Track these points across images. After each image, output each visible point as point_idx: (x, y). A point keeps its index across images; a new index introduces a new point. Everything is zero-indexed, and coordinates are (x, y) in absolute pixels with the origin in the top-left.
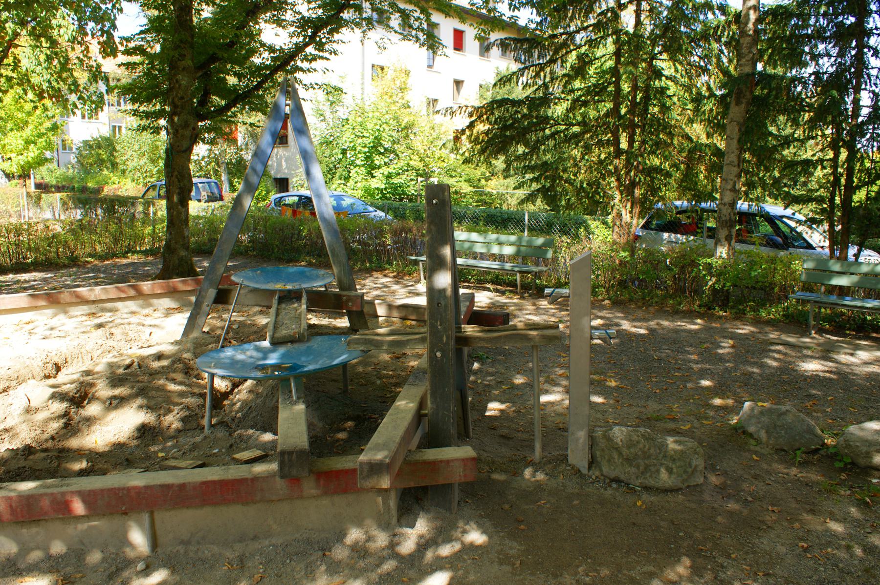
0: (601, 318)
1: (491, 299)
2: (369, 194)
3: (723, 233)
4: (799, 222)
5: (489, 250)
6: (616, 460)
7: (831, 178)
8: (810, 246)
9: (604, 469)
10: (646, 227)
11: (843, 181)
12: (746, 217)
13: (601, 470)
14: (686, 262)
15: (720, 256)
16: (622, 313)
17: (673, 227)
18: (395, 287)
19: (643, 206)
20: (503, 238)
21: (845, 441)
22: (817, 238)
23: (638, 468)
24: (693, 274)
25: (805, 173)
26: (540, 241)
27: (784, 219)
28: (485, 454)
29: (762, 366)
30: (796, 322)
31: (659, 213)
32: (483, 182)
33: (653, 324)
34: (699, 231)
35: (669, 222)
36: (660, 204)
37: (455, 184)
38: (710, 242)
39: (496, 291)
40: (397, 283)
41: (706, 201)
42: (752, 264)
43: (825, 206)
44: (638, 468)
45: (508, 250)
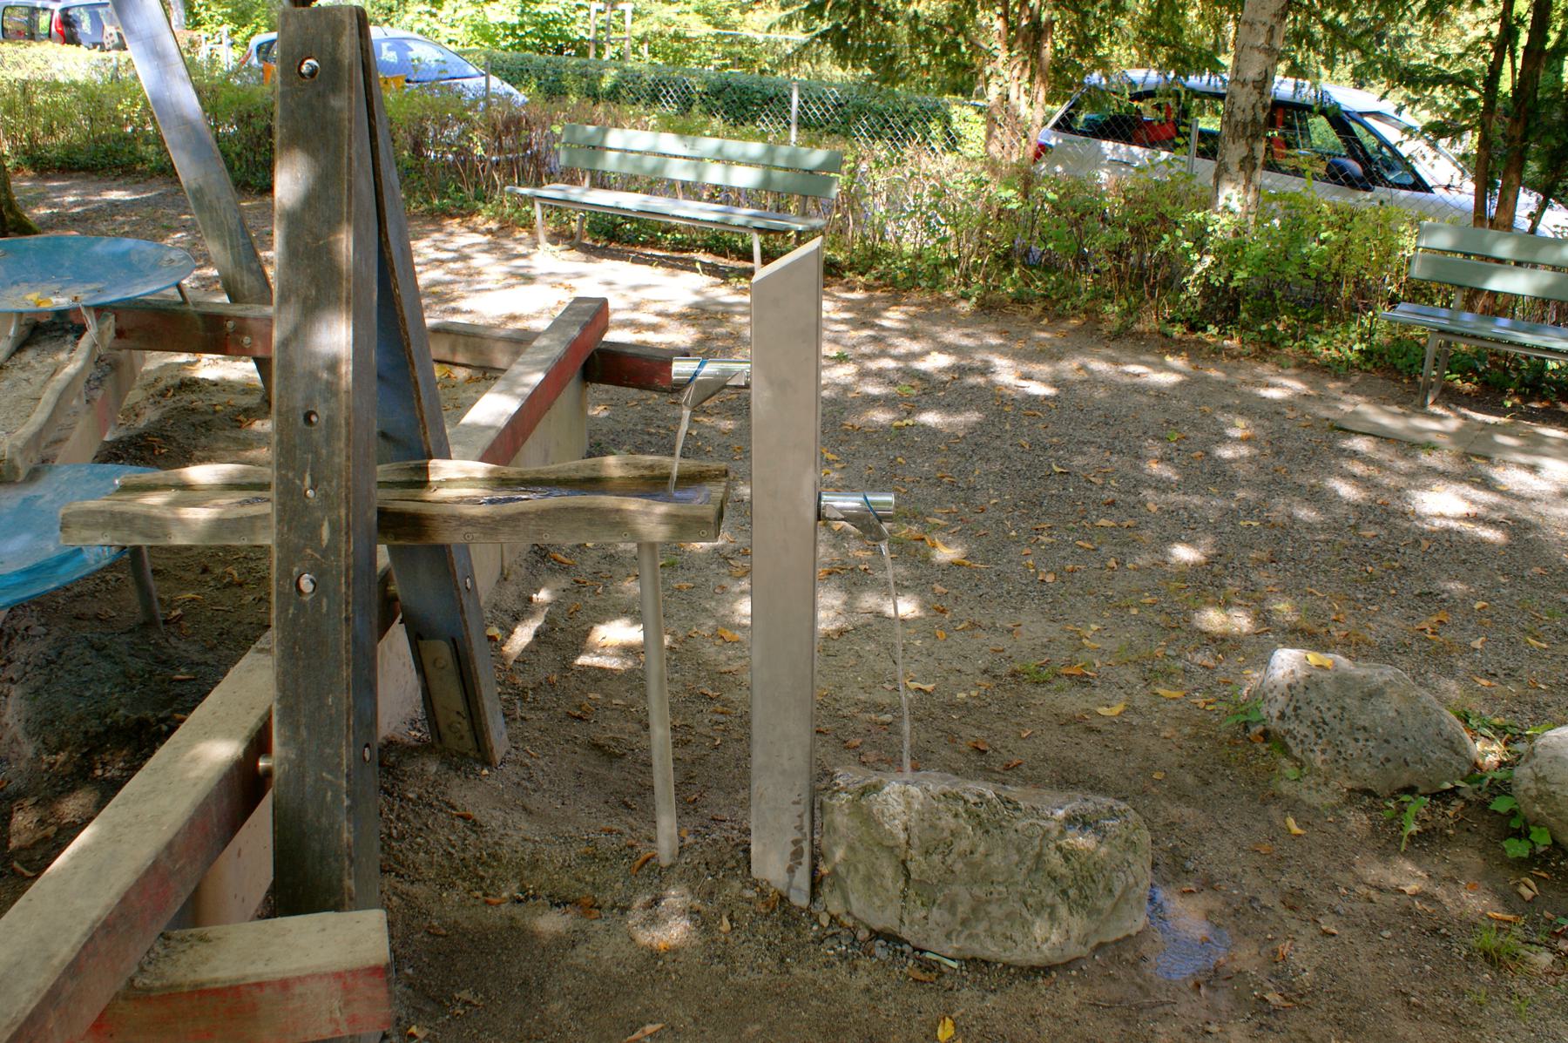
0: (944, 348)
1: (698, 292)
2: (485, 36)
3: (1234, 152)
4: (1408, 130)
5: (700, 175)
6: (889, 883)
7: (1495, 29)
8: (1419, 185)
9: (852, 898)
10: (1065, 125)
11: (1523, 39)
12: (1289, 114)
13: (846, 900)
14: (1151, 216)
15: (1226, 207)
16: (1002, 333)
17: (1122, 128)
18: (481, 260)
19: (1059, 78)
20: (734, 147)
21: (1537, 779)
22: (1444, 170)
23: (952, 908)
24: (1162, 247)
25: (1433, 15)
26: (817, 157)
27: (1369, 120)
28: (526, 827)
29: (1316, 496)
30: (1396, 371)
31: (1095, 96)
32: (735, 15)
33: (1069, 367)
34: (1180, 141)
35: (1114, 118)
36: (1096, 75)
37: (675, 18)
38: (1206, 167)
39: (712, 270)
40: (491, 249)
41: (1200, 72)
42: (1297, 228)
43: (1473, 95)
44: (952, 908)
45: (746, 178)
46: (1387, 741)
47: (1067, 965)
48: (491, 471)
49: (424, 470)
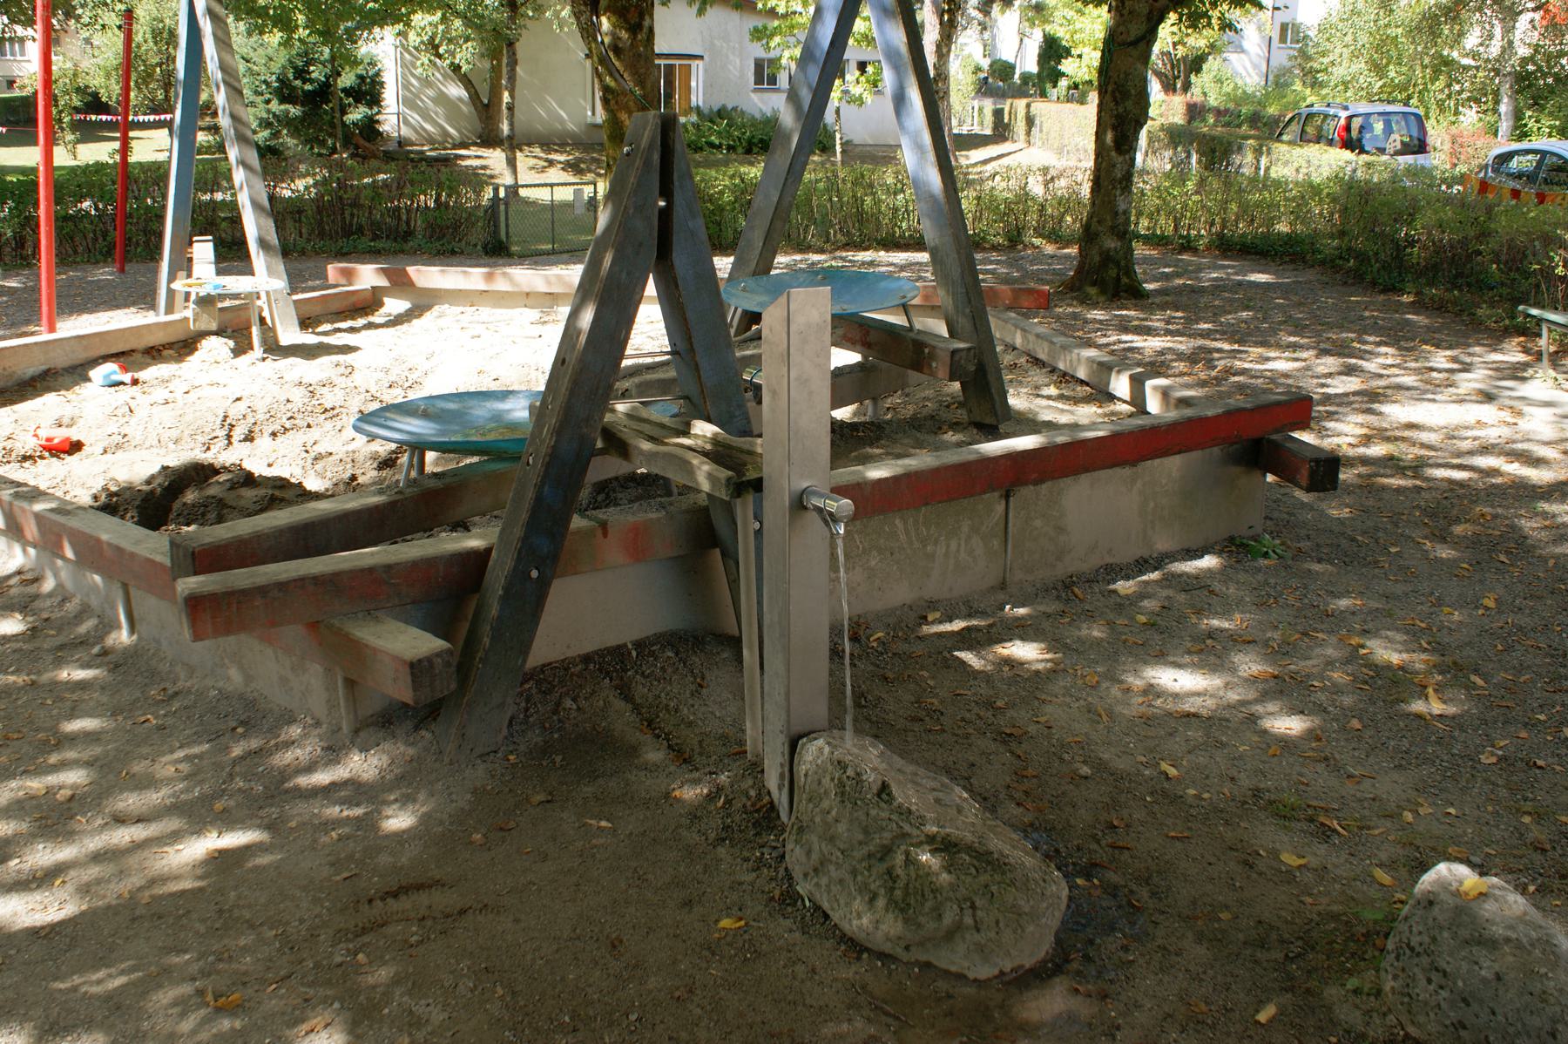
46: (1464, 1000)
47: (882, 956)
48: (716, 434)
49: (688, 425)
